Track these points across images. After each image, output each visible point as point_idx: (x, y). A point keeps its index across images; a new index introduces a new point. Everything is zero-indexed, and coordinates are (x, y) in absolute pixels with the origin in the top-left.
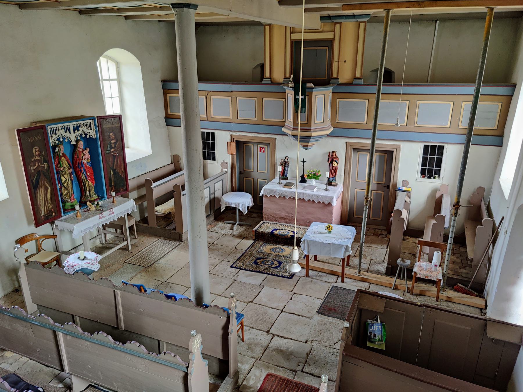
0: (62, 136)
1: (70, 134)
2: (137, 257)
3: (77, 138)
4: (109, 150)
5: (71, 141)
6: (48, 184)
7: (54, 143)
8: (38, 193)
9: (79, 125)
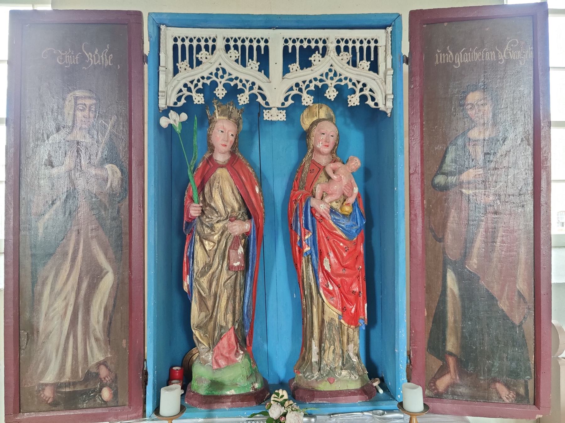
1: (267, 74)
3: (298, 98)
5: (263, 103)
7: (183, 101)
9: (313, 45)
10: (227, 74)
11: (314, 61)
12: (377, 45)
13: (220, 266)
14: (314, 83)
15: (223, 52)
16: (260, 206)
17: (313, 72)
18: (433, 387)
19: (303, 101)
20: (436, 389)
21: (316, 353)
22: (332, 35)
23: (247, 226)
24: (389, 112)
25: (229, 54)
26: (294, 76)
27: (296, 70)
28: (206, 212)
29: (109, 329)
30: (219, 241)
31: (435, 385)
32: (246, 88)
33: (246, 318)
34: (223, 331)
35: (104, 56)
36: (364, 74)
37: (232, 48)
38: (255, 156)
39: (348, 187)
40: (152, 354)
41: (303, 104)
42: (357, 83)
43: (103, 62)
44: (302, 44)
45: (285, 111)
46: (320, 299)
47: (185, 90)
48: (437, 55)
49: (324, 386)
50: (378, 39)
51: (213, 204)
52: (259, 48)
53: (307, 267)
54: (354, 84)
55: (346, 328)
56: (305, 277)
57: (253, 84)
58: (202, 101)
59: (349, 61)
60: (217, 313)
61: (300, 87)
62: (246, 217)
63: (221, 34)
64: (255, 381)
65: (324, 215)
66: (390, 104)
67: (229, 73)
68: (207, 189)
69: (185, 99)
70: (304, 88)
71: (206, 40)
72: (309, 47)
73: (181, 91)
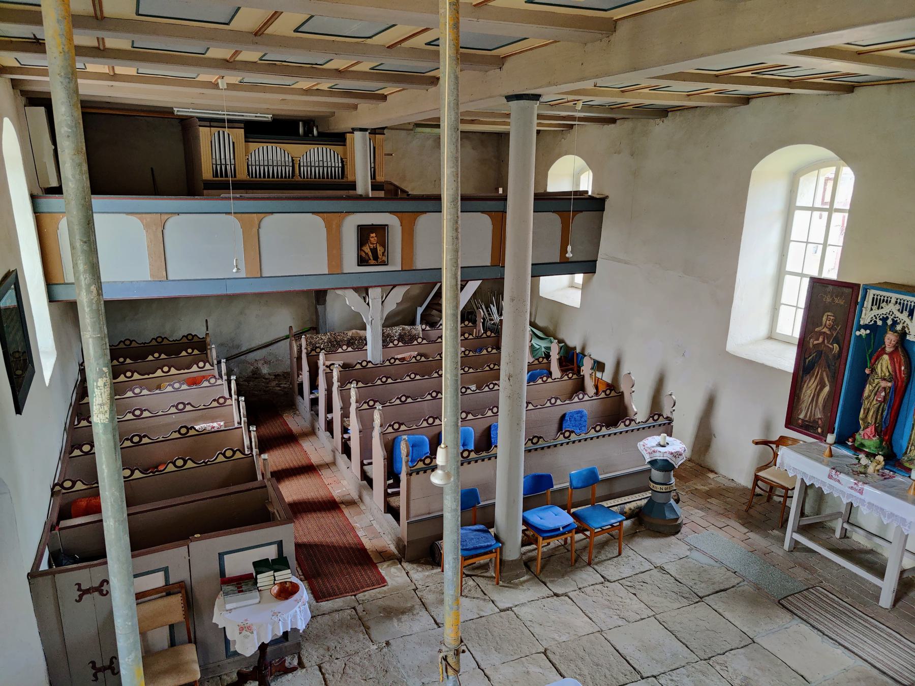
0: (893, 315)
6: (828, 379)
7: (873, 322)
8: (807, 382)
29: (824, 406)
30: (875, 387)
47: (874, 318)
73: (872, 318)
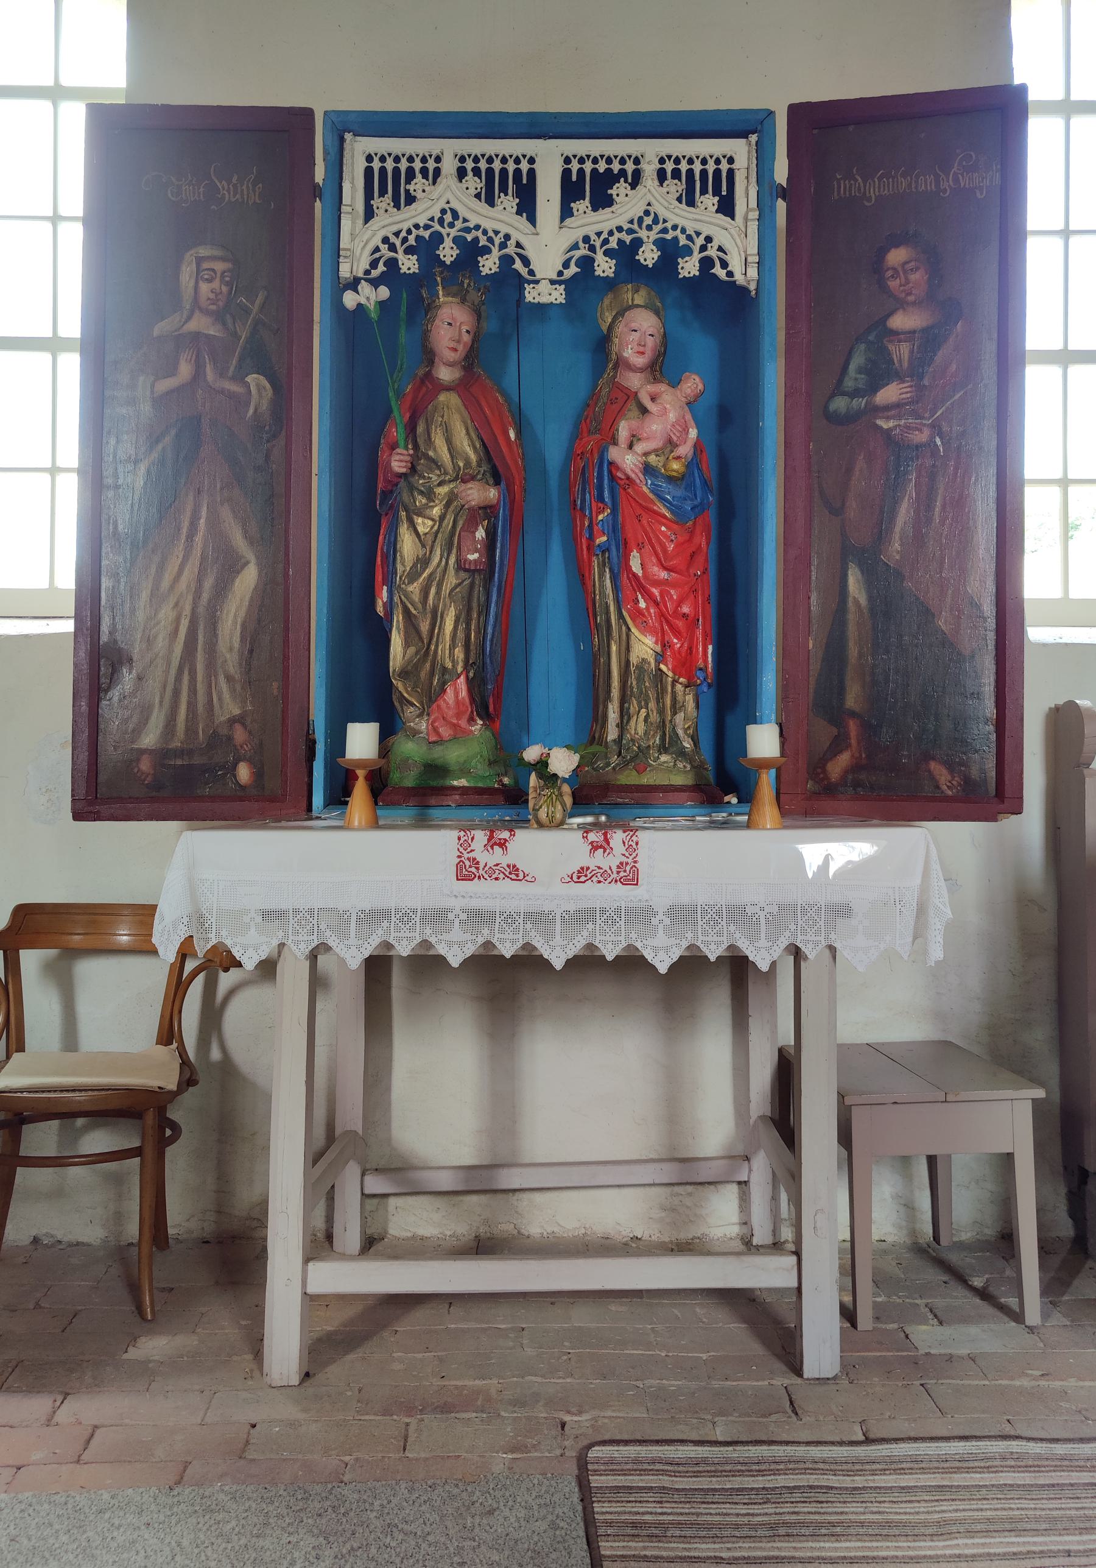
1: (532, 220)
2: (751, 1473)
3: (586, 263)
4: (855, 394)
5: (523, 271)
7: (381, 268)
9: (616, 167)
10: (461, 220)
11: (618, 195)
12: (733, 166)
13: (444, 560)
14: (617, 235)
15: (453, 181)
16: (517, 462)
17: (615, 215)
18: (822, 776)
19: (596, 268)
20: (827, 778)
21: (614, 724)
22: (651, 150)
23: (492, 494)
24: (752, 287)
25: (464, 185)
26: (579, 223)
27: (585, 212)
28: (419, 468)
31: (824, 771)
32: (494, 245)
33: (488, 661)
34: (447, 677)
35: (248, 187)
36: (708, 219)
37: (470, 173)
38: (510, 382)
39: (678, 427)
40: (324, 706)
41: (597, 273)
42: (694, 236)
43: (245, 197)
44: (597, 166)
45: (563, 286)
46: (624, 628)
47: (384, 248)
48: (835, 183)
49: (629, 778)
50: (734, 155)
51: (431, 453)
52: (517, 172)
53: (602, 575)
54: (689, 238)
55: (670, 679)
56: (597, 592)
57: (507, 237)
58: (415, 269)
59: (681, 194)
60: (437, 646)
61: (592, 242)
62: (491, 481)
63: (450, 149)
64: (504, 773)
65: (633, 476)
66: (753, 273)
67: (464, 218)
68: (420, 429)
69: (385, 264)
70: (598, 244)
71: (424, 160)
72: (609, 171)
73: (377, 249)
